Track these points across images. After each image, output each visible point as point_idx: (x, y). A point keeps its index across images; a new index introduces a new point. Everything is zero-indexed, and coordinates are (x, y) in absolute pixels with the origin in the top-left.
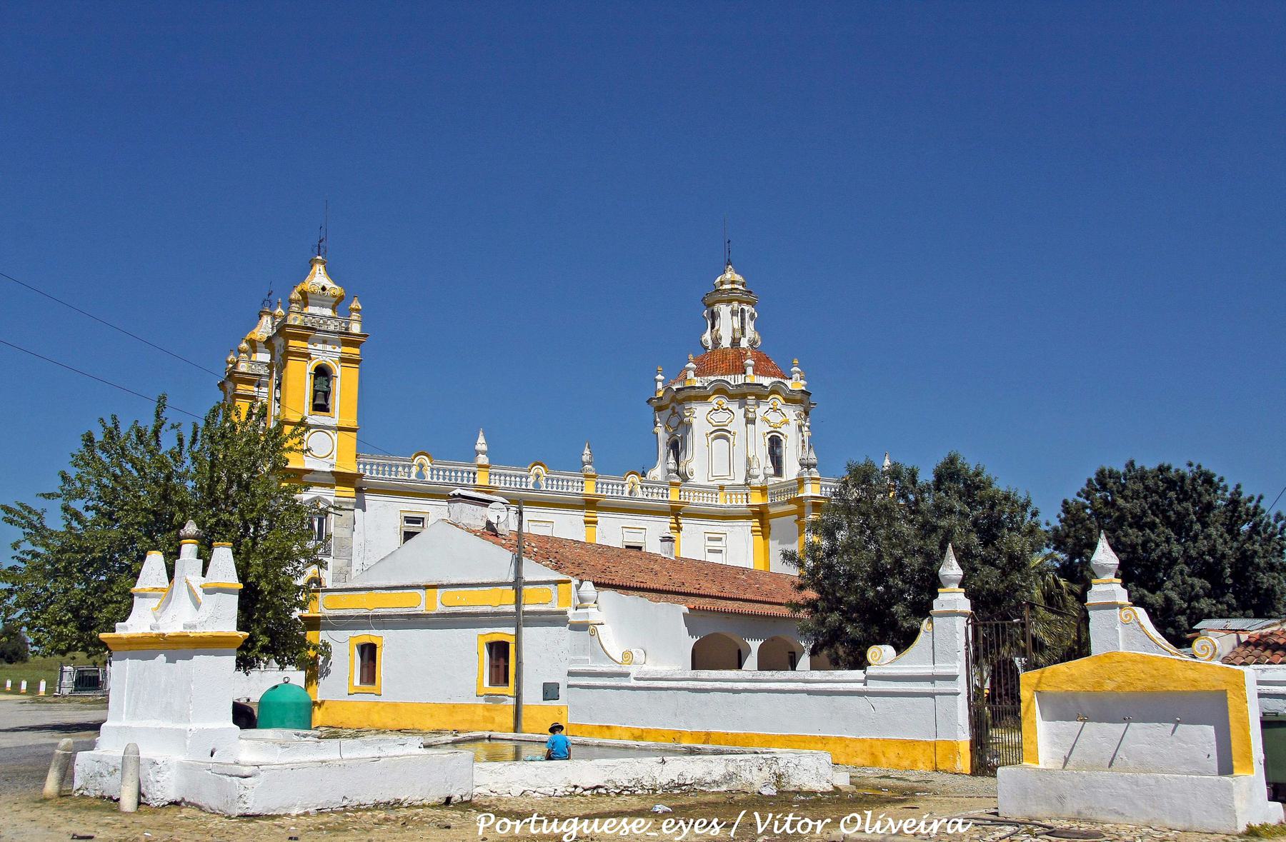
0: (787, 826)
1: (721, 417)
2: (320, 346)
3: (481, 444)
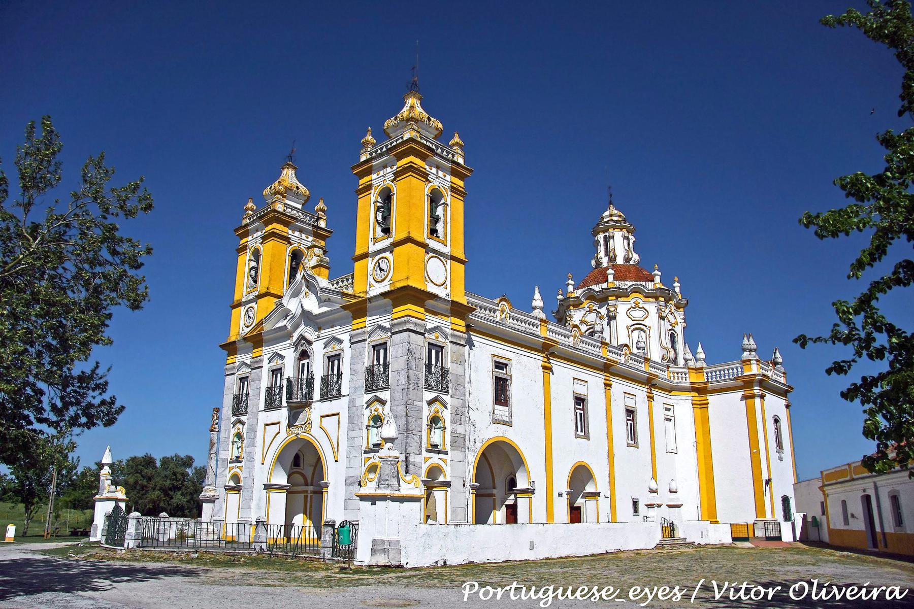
0: (742, 593)
1: (638, 314)
2: (297, 234)
3: (538, 301)
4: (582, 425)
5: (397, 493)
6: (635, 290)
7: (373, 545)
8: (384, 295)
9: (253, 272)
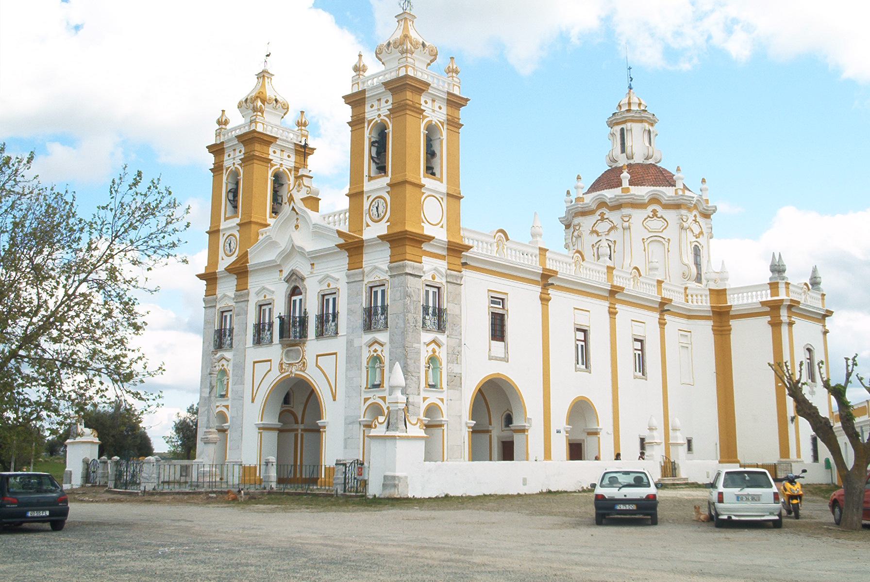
1: (656, 224)
4: (584, 355)
5: (404, 434)
6: (654, 200)
7: (385, 480)
8: (382, 238)
9: (231, 197)
